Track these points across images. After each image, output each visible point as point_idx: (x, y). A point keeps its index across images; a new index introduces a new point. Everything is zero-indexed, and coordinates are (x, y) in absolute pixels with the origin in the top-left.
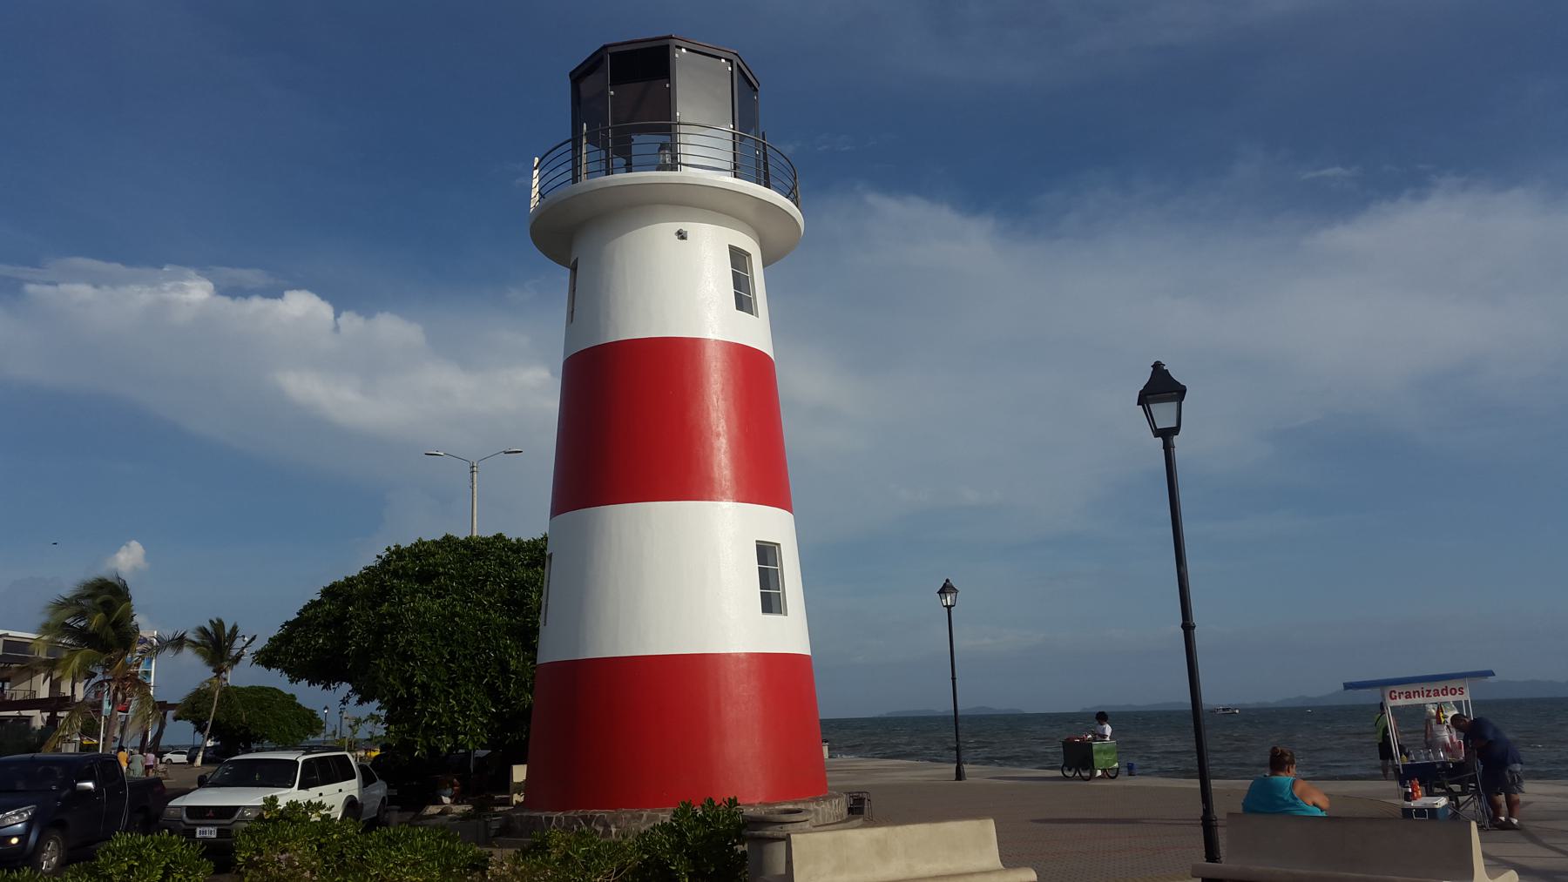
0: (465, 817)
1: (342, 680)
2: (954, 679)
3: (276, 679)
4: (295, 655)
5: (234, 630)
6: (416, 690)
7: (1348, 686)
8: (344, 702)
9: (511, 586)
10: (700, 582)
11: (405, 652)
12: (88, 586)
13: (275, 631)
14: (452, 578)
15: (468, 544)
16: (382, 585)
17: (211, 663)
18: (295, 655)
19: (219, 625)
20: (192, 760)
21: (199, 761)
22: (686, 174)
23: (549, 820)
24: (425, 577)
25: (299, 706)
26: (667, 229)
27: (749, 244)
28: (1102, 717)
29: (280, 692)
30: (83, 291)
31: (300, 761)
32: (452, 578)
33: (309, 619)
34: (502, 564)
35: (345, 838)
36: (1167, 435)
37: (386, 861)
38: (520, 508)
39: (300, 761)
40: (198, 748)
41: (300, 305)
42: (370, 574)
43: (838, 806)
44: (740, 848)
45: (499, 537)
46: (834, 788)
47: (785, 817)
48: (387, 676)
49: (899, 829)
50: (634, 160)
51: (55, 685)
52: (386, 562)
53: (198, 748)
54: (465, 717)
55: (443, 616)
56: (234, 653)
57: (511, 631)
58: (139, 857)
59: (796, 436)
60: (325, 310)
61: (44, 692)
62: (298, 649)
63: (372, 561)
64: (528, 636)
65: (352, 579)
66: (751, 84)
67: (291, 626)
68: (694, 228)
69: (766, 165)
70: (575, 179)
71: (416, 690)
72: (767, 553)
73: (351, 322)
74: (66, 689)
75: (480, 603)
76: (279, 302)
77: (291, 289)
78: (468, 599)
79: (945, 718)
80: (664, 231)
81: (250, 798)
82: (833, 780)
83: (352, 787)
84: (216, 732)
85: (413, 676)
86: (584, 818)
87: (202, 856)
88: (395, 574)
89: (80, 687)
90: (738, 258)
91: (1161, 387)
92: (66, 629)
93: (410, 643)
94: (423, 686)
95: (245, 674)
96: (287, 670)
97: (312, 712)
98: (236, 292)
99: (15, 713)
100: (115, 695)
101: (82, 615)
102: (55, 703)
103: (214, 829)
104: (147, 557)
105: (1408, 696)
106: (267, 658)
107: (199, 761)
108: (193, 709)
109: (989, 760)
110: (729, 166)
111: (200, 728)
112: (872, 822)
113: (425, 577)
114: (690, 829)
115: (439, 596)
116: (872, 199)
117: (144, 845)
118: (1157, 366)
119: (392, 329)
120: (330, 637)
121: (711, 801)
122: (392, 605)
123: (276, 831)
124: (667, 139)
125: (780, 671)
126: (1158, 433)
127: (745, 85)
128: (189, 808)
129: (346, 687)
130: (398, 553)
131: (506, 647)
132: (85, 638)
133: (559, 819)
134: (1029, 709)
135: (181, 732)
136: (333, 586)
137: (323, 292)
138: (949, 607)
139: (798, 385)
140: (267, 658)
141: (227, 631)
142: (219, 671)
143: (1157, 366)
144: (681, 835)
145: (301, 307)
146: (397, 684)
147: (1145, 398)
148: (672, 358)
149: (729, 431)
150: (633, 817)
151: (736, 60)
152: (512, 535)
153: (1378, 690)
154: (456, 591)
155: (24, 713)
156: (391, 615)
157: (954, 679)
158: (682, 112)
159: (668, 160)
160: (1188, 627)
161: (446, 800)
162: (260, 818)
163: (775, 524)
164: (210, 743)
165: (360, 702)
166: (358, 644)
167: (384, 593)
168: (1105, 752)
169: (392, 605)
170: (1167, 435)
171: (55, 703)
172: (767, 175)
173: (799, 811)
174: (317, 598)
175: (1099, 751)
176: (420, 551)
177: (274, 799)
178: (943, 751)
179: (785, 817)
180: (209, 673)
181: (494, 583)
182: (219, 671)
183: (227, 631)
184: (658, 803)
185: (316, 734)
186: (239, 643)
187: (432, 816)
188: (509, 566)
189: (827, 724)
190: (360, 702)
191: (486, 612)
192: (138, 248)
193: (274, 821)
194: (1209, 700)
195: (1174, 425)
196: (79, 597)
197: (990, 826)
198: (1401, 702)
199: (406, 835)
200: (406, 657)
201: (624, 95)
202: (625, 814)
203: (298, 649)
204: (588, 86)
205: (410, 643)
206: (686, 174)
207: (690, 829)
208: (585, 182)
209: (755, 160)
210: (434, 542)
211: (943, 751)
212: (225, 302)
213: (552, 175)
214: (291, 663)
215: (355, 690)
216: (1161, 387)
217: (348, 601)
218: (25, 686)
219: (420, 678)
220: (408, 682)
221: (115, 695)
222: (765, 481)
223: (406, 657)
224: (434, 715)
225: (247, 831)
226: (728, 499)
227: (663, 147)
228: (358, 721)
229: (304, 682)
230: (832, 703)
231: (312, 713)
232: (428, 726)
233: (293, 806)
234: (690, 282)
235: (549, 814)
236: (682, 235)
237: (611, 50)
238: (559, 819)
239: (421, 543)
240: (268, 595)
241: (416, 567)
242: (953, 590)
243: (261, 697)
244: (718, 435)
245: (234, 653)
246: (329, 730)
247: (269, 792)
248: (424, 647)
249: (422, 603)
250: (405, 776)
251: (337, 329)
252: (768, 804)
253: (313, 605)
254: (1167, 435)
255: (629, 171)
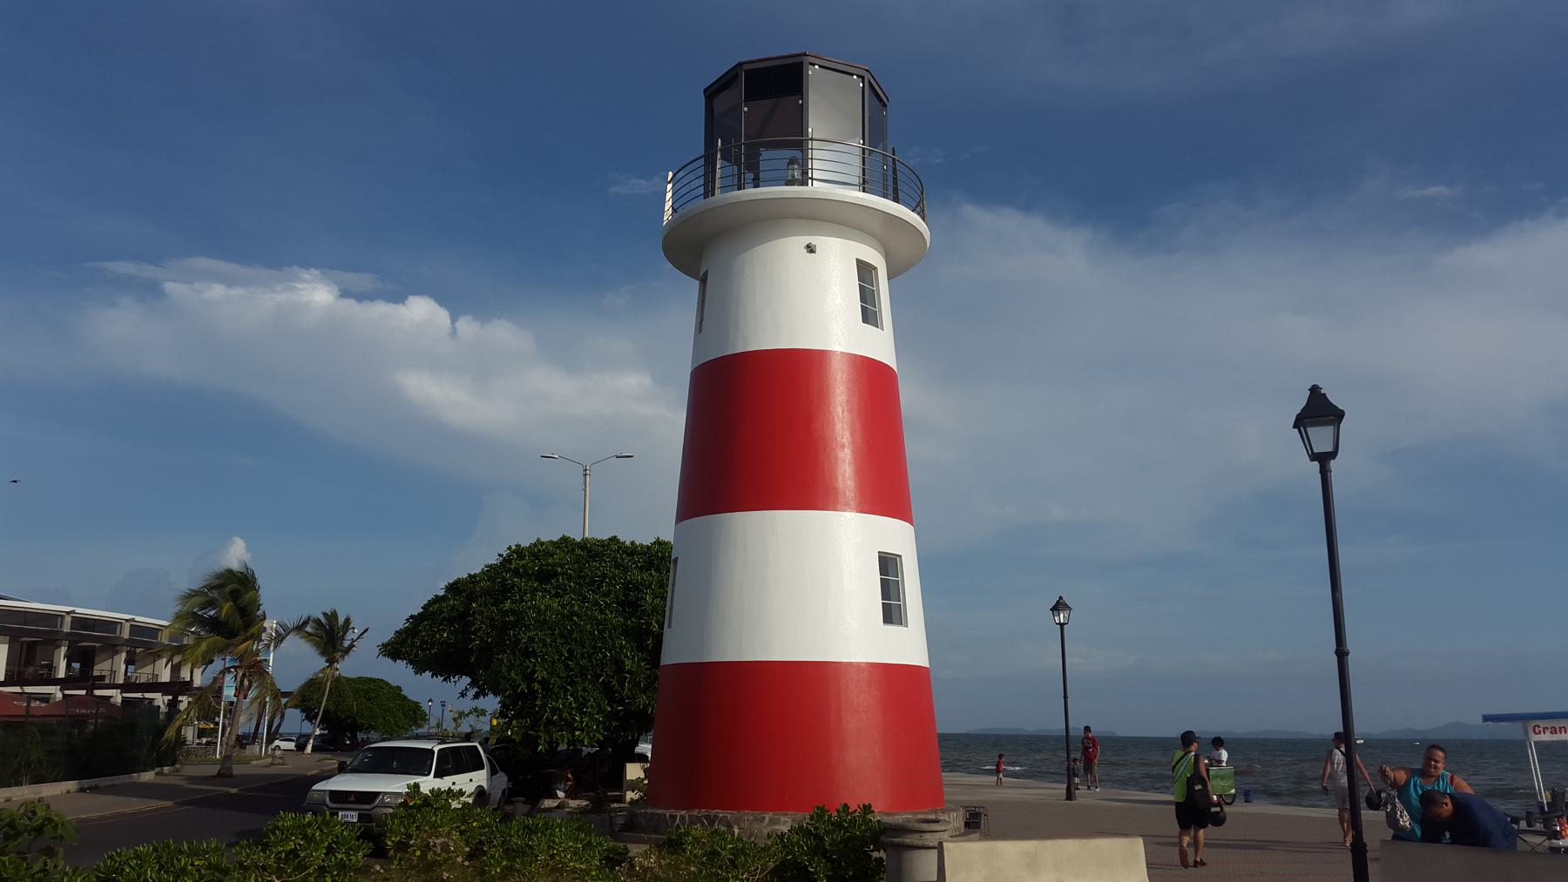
0: (583, 811)
1: (462, 674)
2: (1065, 697)
3: (399, 674)
4: (420, 648)
5: (347, 621)
6: (536, 686)
7: (1486, 718)
8: (463, 695)
9: (626, 587)
10: (822, 590)
11: (527, 648)
12: (219, 576)
13: (401, 624)
14: (570, 578)
15: (585, 545)
16: (503, 584)
17: (323, 654)
18: (420, 648)
19: (332, 617)
20: (301, 747)
21: (309, 748)
22: (817, 189)
23: (673, 818)
24: (545, 576)
25: (405, 698)
26: (797, 243)
27: (875, 258)
28: (1218, 742)
29: (387, 684)
30: (218, 291)
31: (436, 750)
32: (570, 578)
33: (434, 614)
34: (617, 566)
35: (483, 827)
36: (1323, 460)
37: (550, 847)
38: (644, 509)
39: (436, 750)
40: (308, 737)
41: (421, 311)
42: (491, 572)
43: (956, 819)
44: (875, 854)
45: (614, 539)
46: (951, 802)
47: (925, 826)
48: (509, 671)
49: (1048, 843)
50: (762, 175)
51: (176, 670)
52: (506, 561)
53: (308, 737)
54: (583, 714)
55: (563, 615)
56: (346, 644)
57: (626, 632)
58: (305, 837)
59: (916, 450)
60: (443, 316)
61: (165, 676)
62: (423, 642)
63: (493, 560)
64: (649, 641)
65: (475, 576)
66: (880, 100)
67: (416, 620)
68: (822, 242)
69: (895, 180)
70: (709, 192)
71: (536, 686)
72: (888, 564)
73: (468, 327)
74: (185, 674)
75: (596, 604)
76: (401, 307)
77: (414, 294)
78: (584, 599)
79: (1056, 738)
80: (793, 245)
81: (394, 785)
82: (949, 794)
83: (480, 778)
84: (327, 721)
85: (534, 672)
86: (707, 817)
87: (358, 839)
88: (516, 573)
89: (198, 672)
90: (865, 270)
91: (1319, 411)
92: (195, 618)
93: (531, 639)
94: (544, 683)
95: (364, 661)
96: (411, 662)
97: (416, 704)
98: (361, 297)
99: (139, 695)
100: (242, 682)
101: (211, 603)
102: (177, 687)
103: (355, 814)
104: (248, 549)
105: (1554, 731)
106: (393, 650)
107: (309, 748)
108: (306, 700)
109: (1124, 783)
110: (856, 181)
111: (310, 717)
112: (987, 836)
113: (545, 576)
114: (827, 833)
115: (557, 595)
116: (970, 211)
117: (309, 824)
118: (1315, 390)
119: (504, 334)
120: (451, 632)
121: (823, 810)
122: (514, 602)
123: (424, 818)
124: (797, 154)
125: (900, 684)
126: (1314, 457)
127: (875, 98)
128: (332, 792)
129: (466, 680)
130: (519, 552)
131: (622, 647)
132: (214, 625)
133: (683, 817)
134: (1121, 734)
135: (294, 720)
136: (457, 582)
137: (442, 299)
138: (1062, 625)
139: (911, 398)
140: (393, 650)
141: (341, 620)
142: (332, 661)
143: (1315, 390)
144: (819, 838)
145: (421, 312)
146: (518, 679)
147: (1301, 422)
148: (797, 370)
149: (853, 442)
150: (755, 819)
151: (867, 76)
152: (626, 538)
153: (1518, 725)
154: (573, 591)
155: (148, 695)
156: (513, 612)
157: (1065, 697)
158: (815, 127)
159: (797, 174)
160: (1341, 654)
161: (561, 794)
162: (404, 804)
163: (897, 535)
164: (318, 732)
165: (476, 696)
166: (482, 639)
167: (506, 591)
168: (1222, 778)
169: (514, 602)
170: (1324, 459)
171: (177, 687)
172: (896, 191)
173: (936, 821)
174: (442, 593)
175: (1216, 777)
176: (538, 551)
177: (417, 786)
178: (1072, 770)
179: (925, 826)
180: (321, 662)
181: (609, 585)
182: (332, 661)
183: (341, 620)
184: (782, 806)
185: (421, 726)
186: (350, 636)
187: (550, 810)
188: (626, 570)
189: (944, 738)
190: (476, 696)
191: (602, 612)
192: (267, 250)
193: (418, 808)
194: (1364, 727)
195: (1330, 449)
196: (211, 587)
197: (1138, 845)
198: (1546, 737)
199: (546, 824)
200: (527, 654)
201: (756, 110)
202: (748, 816)
203: (423, 642)
204: (721, 104)
205: (531, 639)
206: (817, 189)
207: (827, 833)
208: (720, 197)
209: (885, 175)
210: (551, 542)
211: (1072, 770)
212: (350, 304)
213: (683, 191)
214: (416, 655)
215: (473, 684)
216: (1319, 411)
217: (472, 597)
218: (148, 669)
219: (540, 674)
220: (529, 678)
221: (242, 682)
222: (886, 493)
223: (527, 654)
224: (554, 710)
225: (393, 816)
226: (852, 510)
227: (792, 161)
228: (461, 715)
229: (428, 674)
230: (950, 717)
231: (417, 706)
232: (550, 722)
233: (437, 793)
234: (817, 296)
235: (672, 812)
236: (811, 249)
237: (745, 67)
238: (683, 817)
239: (539, 543)
240: (385, 588)
241: (535, 567)
242: (1066, 607)
243: (371, 689)
244: (843, 446)
245: (346, 644)
246: (433, 722)
247: (413, 780)
248: (545, 645)
249: (542, 600)
250: (525, 767)
251: (454, 332)
252: (888, 814)
253: (437, 600)
254: (1324, 459)
255: (756, 186)
